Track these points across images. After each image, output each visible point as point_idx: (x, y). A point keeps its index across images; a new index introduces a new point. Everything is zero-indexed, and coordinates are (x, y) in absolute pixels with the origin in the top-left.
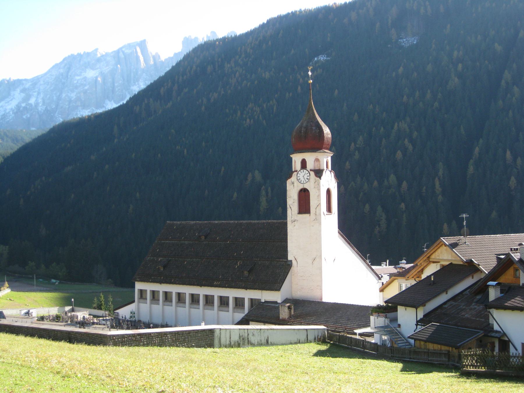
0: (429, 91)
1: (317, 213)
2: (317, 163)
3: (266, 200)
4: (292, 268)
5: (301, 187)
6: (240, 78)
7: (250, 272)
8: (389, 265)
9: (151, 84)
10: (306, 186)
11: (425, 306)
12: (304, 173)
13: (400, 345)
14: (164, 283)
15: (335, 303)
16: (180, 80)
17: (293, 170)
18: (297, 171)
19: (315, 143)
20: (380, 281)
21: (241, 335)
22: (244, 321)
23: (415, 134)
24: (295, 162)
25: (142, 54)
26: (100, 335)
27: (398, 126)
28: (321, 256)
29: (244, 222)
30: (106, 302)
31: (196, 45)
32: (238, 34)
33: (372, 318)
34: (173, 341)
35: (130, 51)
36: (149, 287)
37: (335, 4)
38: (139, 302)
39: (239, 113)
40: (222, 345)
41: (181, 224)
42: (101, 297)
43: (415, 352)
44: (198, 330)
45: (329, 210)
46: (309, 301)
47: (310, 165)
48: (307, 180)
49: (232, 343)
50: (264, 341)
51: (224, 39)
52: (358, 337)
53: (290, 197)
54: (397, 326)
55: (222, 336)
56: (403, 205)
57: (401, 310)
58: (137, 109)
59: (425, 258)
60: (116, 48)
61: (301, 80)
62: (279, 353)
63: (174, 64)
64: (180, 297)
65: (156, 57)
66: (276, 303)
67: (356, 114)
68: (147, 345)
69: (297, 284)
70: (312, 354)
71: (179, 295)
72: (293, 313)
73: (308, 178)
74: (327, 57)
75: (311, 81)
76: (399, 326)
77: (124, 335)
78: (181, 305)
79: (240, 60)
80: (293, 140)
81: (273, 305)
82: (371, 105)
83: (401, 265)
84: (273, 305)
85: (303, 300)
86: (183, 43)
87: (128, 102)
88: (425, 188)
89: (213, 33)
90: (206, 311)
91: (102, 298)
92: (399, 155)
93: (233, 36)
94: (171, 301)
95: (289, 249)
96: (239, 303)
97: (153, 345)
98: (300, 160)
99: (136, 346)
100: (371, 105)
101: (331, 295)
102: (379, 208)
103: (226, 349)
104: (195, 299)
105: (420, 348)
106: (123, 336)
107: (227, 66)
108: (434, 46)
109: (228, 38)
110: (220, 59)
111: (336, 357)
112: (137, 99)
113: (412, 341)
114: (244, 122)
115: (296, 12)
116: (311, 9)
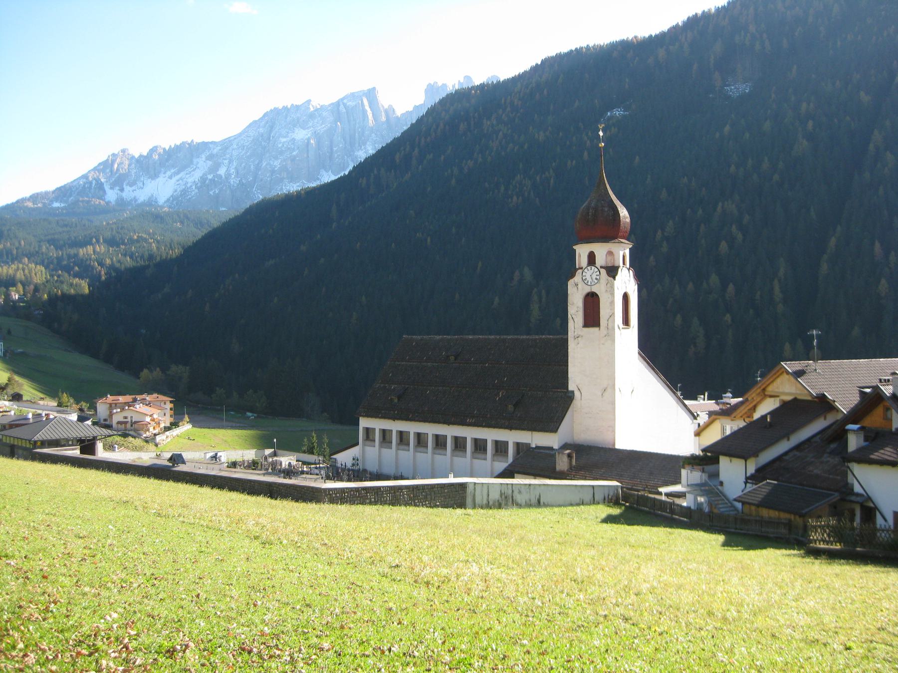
0: (766, 159)
2: (609, 258)
5: (587, 290)
10: (595, 289)
11: (757, 456)
16: (423, 140)
19: (607, 230)
22: (508, 473)
23: (746, 218)
24: (580, 256)
26: (313, 488)
27: (722, 207)
28: (614, 385)
30: (320, 444)
31: (444, 95)
33: (684, 472)
36: (378, 424)
37: (635, 37)
38: (364, 445)
39: (502, 188)
41: (422, 340)
44: (444, 484)
45: (626, 321)
47: (600, 260)
49: (491, 503)
50: (534, 501)
51: (482, 86)
52: (663, 498)
53: (573, 304)
56: (728, 317)
57: (724, 461)
58: (363, 182)
59: (759, 391)
60: (335, 100)
62: (554, 518)
63: (414, 121)
65: (390, 111)
66: (551, 449)
68: (375, 503)
71: (418, 435)
72: (574, 463)
76: (721, 483)
83: (725, 400)
86: (426, 91)
88: (759, 293)
90: (455, 459)
92: (724, 246)
94: (408, 444)
96: (500, 448)
97: (384, 503)
98: (587, 254)
102: (696, 321)
105: (750, 515)
106: (342, 490)
111: (633, 525)
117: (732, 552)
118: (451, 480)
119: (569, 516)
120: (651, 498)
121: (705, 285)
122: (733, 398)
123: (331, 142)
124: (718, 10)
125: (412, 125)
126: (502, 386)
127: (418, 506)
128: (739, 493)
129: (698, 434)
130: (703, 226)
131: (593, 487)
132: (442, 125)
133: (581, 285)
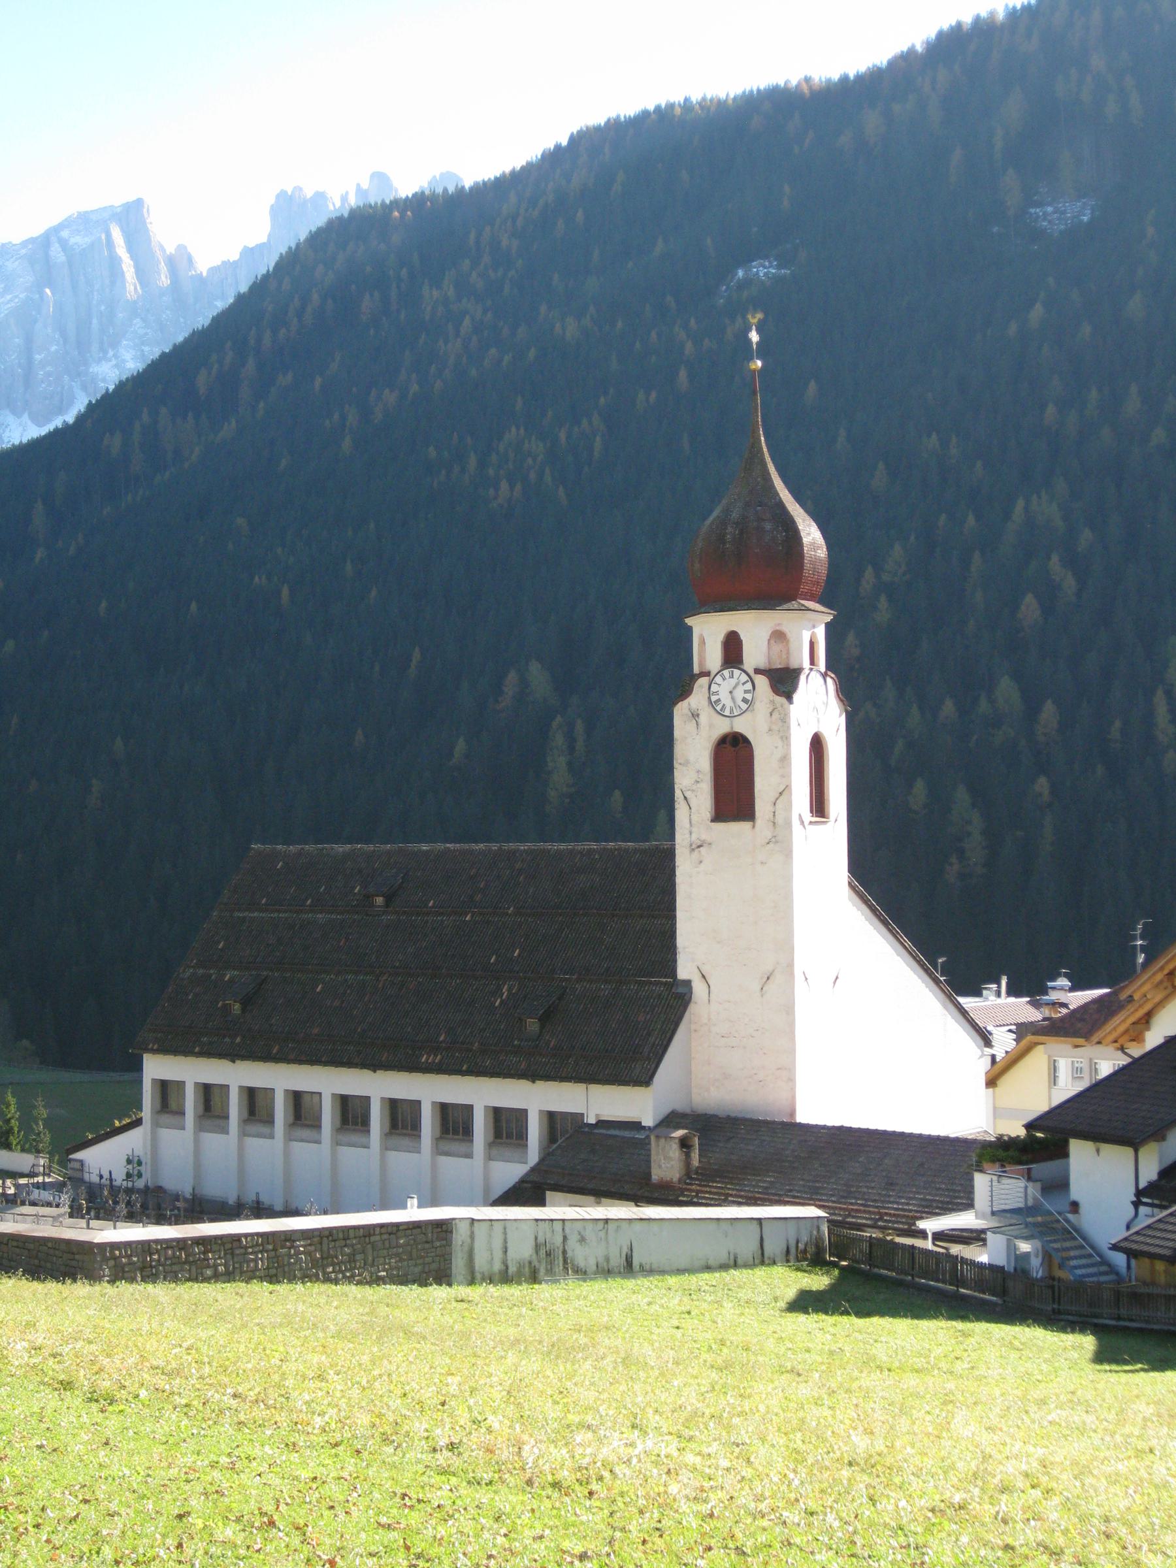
0: (1134, 389)
1: (780, 819)
2: (777, 648)
3: (570, 764)
4: (692, 1008)
5: (723, 727)
6: (475, 338)
7: (544, 1020)
8: (1010, 993)
9: (163, 356)
10: (741, 726)
11: (1163, 1138)
12: (733, 681)
13: (1079, 1272)
14: (244, 1058)
15: (841, 1129)
16: (267, 340)
17: (696, 670)
18: (708, 674)
19: (770, 578)
20: (988, 1051)
21: (541, 1239)
22: (527, 1192)
23: (1086, 536)
24: (703, 642)
25: (130, 250)
26: (69, 1242)
27: (1026, 508)
28: (791, 965)
29: (523, 847)
30: (27, 1121)
31: (320, 221)
32: (468, 184)
33: (981, 1182)
34: (315, 1263)
35: (88, 240)
36: (191, 1072)
37: (807, 80)
38: (156, 1125)
39: (473, 461)
40: (478, 1276)
41: (300, 854)
42: (8, 1105)
43: (1136, 1297)
44: (397, 1225)
45: (819, 807)
46: (751, 1120)
47: (755, 653)
48: (744, 706)
49: (512, 1269)
50: (617, 1261)
51: (419, 202)
52: (928, 1245)
53: (686, 763)
54: (1068, 1208)
55: (477, 1245)
56: (1042, 785)
57: (1080, 1152)
58: (114, 443)
59: (1159, 977)
60: (37, 230)
61: (689, 347)
62: (675, 1302)
63: (244, 288)
64: (302, 1109)
65: (179, 262)
66: (637, 1126)
67: (881, 465)
68: (229, 1276)
69: (707, 1064)
70: (782, 1304)
71: (297, 1099)
72: (695, 1162)
73: (749, 696)
74: (779, 267)
75: (759, 363)
76: (1075, 1206)
77: (149, 1242)
78: (306, 1133)
79: (474, 275)
80: (697, 566)
81: (627, 1134)
82: (934, 436)
83: (1054, 996)
84: (627, 1134)
85: (728, 1118)
86: (275, 211)
87: (81, 419)
88: (1118, 724)
89: (380, 178)
90: (393, 1156)
91: (13, 1109)
92: (1030, 608)
93: (451, 190)
94: (270, 1121)
95: (681, 941)
96: (507, 1127)
97: (250, 1276)
98: (721, 637)
99: (189, 1280)
100: (934, 436)
101: (827, 1096)
102: (962, 795)
103: (492, 1289)
104: (352, 1114)
105: (1153, 1283)
106: (145, 1247)
107: (430, 295)
108: (1150, 231)
109: (433, 197)
110: (404, 272)
111: (868, 1314)
112: (112, 409)
113: (1119, 1259)
114: (492, 492)
115: (671, 106)
116: (723, 96)
117: (1124, 1377)
118: (413, 1213)
119: (708, 1298)
120: (904, 1246)
121: (984, 706)
122: (1072, 989)
123: (29, 340)
124: (1014, 15)
125: (240, 299)
126: (532, 970)
127: (336, 1282)
128: (1119, 1234)
129: (991, 1082)
130: (977, 557)
131: (760, 1221)
132: (315, 297)
133: (706, 715)
